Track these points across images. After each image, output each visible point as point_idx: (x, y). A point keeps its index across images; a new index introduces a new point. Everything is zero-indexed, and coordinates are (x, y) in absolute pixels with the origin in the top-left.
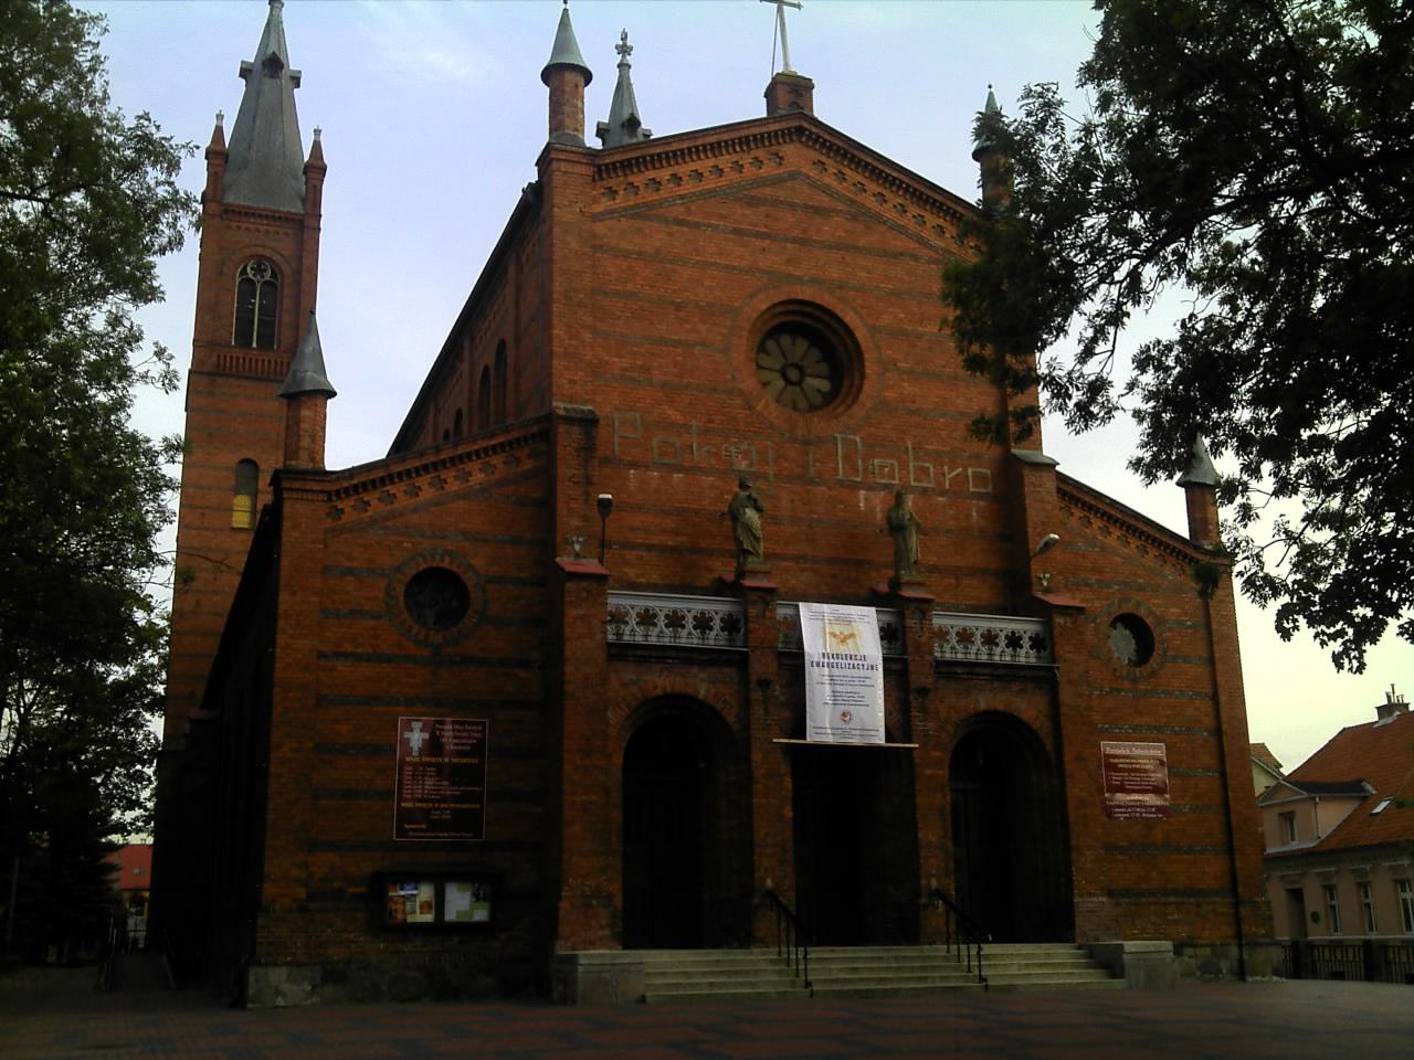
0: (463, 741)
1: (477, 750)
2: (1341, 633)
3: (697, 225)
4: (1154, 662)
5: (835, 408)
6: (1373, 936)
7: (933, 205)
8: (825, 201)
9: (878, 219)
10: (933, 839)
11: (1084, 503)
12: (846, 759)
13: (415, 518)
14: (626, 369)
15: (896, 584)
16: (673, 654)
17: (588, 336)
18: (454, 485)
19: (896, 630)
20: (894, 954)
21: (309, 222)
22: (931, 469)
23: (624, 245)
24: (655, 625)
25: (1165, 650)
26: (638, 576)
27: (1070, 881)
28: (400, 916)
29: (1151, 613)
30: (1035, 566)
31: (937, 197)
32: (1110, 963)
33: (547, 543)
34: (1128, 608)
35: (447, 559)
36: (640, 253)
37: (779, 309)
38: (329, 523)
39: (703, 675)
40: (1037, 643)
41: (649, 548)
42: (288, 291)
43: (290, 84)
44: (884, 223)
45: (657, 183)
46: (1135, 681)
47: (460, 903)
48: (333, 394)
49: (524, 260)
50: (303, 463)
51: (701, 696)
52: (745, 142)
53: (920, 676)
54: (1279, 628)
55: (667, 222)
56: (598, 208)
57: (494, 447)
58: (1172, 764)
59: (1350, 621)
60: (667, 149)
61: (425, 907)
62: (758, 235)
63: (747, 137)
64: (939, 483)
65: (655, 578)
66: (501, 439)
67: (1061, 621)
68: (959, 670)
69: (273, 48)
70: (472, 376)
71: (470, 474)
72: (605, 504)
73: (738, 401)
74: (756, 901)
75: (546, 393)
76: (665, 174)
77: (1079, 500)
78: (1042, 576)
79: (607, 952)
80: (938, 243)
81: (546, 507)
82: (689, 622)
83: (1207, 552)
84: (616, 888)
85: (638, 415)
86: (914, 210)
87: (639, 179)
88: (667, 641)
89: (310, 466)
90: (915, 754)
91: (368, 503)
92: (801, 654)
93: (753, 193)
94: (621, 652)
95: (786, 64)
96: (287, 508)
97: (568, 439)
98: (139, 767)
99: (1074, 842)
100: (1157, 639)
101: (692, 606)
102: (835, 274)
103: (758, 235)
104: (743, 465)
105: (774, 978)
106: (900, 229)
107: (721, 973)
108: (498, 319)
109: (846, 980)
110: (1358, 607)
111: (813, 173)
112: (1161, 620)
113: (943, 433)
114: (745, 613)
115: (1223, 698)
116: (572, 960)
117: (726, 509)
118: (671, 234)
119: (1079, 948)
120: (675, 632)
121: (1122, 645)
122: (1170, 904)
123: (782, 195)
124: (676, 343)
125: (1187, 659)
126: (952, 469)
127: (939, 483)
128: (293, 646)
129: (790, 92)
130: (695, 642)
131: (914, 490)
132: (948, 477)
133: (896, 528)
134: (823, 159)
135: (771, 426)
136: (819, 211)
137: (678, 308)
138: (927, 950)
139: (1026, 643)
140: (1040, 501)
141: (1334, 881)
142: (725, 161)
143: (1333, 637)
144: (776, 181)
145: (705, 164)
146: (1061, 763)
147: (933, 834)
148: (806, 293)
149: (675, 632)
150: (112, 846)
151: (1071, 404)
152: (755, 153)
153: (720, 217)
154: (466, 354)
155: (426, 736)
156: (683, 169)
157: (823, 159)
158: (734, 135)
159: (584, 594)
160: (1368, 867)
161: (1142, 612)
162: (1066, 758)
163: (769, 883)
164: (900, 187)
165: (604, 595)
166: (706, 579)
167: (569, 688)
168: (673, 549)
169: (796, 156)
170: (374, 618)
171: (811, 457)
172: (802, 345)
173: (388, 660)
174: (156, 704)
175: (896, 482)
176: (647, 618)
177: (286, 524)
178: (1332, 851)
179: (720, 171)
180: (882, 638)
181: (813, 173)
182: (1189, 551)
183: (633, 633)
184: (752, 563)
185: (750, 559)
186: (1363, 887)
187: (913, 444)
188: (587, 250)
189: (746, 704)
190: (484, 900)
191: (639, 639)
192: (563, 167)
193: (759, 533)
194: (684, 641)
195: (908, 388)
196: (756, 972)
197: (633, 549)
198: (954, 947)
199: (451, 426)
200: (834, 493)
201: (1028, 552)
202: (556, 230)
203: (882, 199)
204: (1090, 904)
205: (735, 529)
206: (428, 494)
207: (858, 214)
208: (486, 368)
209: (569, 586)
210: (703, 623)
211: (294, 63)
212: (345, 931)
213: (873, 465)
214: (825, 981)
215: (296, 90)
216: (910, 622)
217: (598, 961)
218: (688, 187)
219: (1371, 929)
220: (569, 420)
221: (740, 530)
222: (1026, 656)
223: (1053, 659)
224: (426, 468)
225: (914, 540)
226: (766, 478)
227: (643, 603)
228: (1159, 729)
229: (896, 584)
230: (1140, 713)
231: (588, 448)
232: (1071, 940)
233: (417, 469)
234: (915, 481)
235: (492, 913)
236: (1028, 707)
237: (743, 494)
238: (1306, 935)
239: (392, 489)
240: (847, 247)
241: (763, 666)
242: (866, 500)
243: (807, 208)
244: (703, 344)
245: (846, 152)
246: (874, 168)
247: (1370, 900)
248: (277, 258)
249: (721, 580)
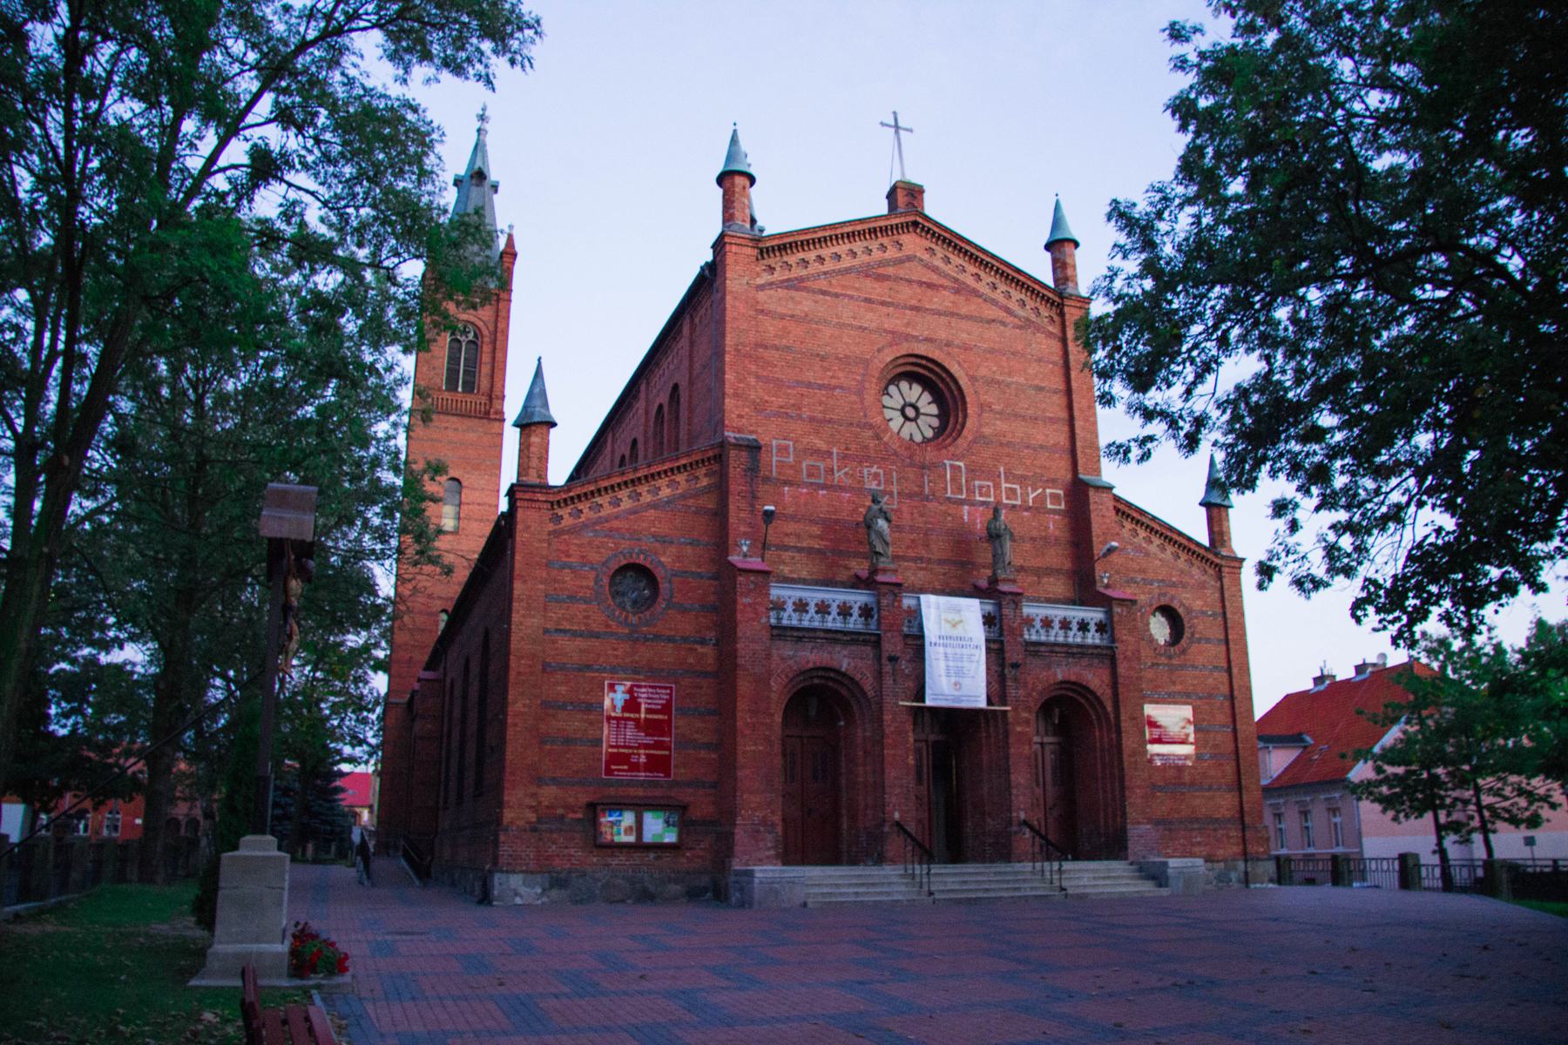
1: (666, 708)
2: (1398, 619)
3: (837, 295)
4: (1184, 642)
5: (944, 440)
6: (1340, 850)
7: (1017, 284)
8: (934, 278)
9: (975, 293)
10: (1022, 781)
11: (1133, 519)
12: (955, 721)
13: (616, 524)
14: (782, 407)
15: (994, 581)
16: (822, 635)
17: (752, 380)
19: (994, 618)
20: (993, 870)
21: (504, 296)
23: (780, 310)
24: (807, 612)
25: (1193, 634)
26: (791, 572)
27: (1124, 814)
28: (609, 837)
29: (1182, 604)
30: (1098, 567)
31: (1021, 278)
32: (1157, 876)
33: (722, 544)
34: (1164, 601)
35: (642, 556)
36: (792, 316)
37: (901, 361)
38: (551, 527)
39: (846, 652)
40: (1101, 628)
41: (800, 550)
42: (486, 349)
43: (491, 191)
44: (980, 296)
45: (805, 263)
46: (1170, 658)
47: (657, 828)
48: (554, 425)
49: (697, 320)
50: (532, 479)
51: (843, 669)
52: (873, 232)
53: (1013, 655)
54: (1353, 615)
55: (814, 292)
56: (760, 281)
57: (678, 468)
58: (1197, 722)
59: (1404, 610)
60: (814, 236)
61: (628, 830)
62: (883, 303)
63: (875, 229)
64: (1025, 501)
65: (804, 574)
66: (683, 462)
67: (1119, 610)
68: (1042, 649)
69: (479, 164)
70: (647, 412)
71: (659, 489)
72: (769, 516)
73: (870, 433)
74: (886, 829)
75: (721, 424)
76: (811, 255)
77: (1128, 516)
78: (1103, 577)
79: (771, 868)
80: (1021, 313)
81: (720, 515)
82: (834, 610)
83: (1223, 557)
84: (777, 818)
85: (791, 443)
86: (1002, 287)
87: (791, 259)
88: (816, 624)
89: (537, 481)
90: (1009, 715)
91: (581, 511)
92: (921, 637)
93: (881, 271)
95: (903, 174)
96: (520, 514)
97: (737, 462)
98: (365, 713)
99: (1127, 784)
100: (1187, 625)
101: (835, 597)
102: (942, 335)
103: (883, 303)
104: (873, 486)
105: (903, 888)
106: (994, 302)
107: (863, 885)
108: (671, 367)
109: (958, 891)
111: (926, 257)
112: (1189, 610)
113: (1028, 462)
114: (879, 603)
115: (1235, 671)
116: (750, 874)
117: (861, 519)
118: (816, 302)
119: (1131, 864)
120: (823, 617)
121: (1159, 629)
122: (1194, 829)
123: (902, 273)
124: (821, 387)
125: (1208, 640)
126: (1034, 490)
127: (1025, 501)
128: (526, 624)
129: (905, 196)
130: (839, 625)
131: (1006, 506)
132: (1031, 496)
133: (994, 536)
134: (933, 246)
135: (895, 454)
136: (930, 286)
137: (823, 359)
138: (1018, 866)
139: (1092, 628)
140: (1101, 516)
141: (1283, 810)
142: (858, 246)
143: (1392, 622)
144: (898, 262)
145: (842, 248)
146: (1117, 717)
147: (1020, 777)
148: (921, 349)
149: (823, 617)
150: (341, 774)
151: (1182, 433)
152: (881, 240)
153: (857, 289)
154: (642, 395)
155: (627, 696)
156: (826, 252)
157: (933, 246)
158: (866, 226)
159: (752, 586)
160: (1308, 799)
161: (1175, 604)
162: (1123, 718)
163: (897, 815)
164: (992, 268)
165: (766, 587)
166: (843, 575)
167: (741, 661)
168: (819, 551)
169: (913, 243)
170: (585, 602)
172: (917, 389)
173: (597, 636)
174: (379, 666)
175: (992, 499)
176: (801, 607)
177: (519, 527)
178: (1281, 788)
179: (853, 254)
180: (984, 624)
181: (926, 257)
182: (1210, 556)
183: (790, 618)
184: (883, 562)
185: (882, 559)
186: (1305, 814)
188: (752, 313)
189: (879, 675)
190: (674, 825)
191: (795, 623)
192: (734, 248)
193: (888, 539)
194: (830, 625)
195: (1001, 425)
196: (890, 884)
197: (786, 550)
198: (1038, 865)
199: (627, 454)
200: (943, 508)
201: (1093, 555)
202: (728, 298)
203: (978, 277)
204: (1140, 833)
205: (869, 535)
207: (959, 289)
208: (661, 406)
209: (740, 579)
210: (845, 611)
211: (494, 175)
212: (567, 847)
214: (943, 891)
215: (495, 196)
216: (1006, 611)
217: (771, 875)
218: (829, 265)
219: (1338, 845)
220: (738, 446)
221: (873, 536)
222: (1093, 638)
223: (1113, 640)
225: (1008, 545)
226: (891, 494)
228: (1188, 695)
229: (994, 581)
230: (1174, 683)
231: (753, 470)
232: (1126, 858)
233: (619, 485)
234: (1007, 498)
235: (680, 836)
236: (1096, 679)
237: (875, 507)
239: (598, 500)
240: (953, 314)
241: (891, 646)
243: (921, 283)
244: (841, 388)
245: (951, 242)
246: (972, 254)
247: (1309, 824)
248: (480, 324)
249: (857, 576)
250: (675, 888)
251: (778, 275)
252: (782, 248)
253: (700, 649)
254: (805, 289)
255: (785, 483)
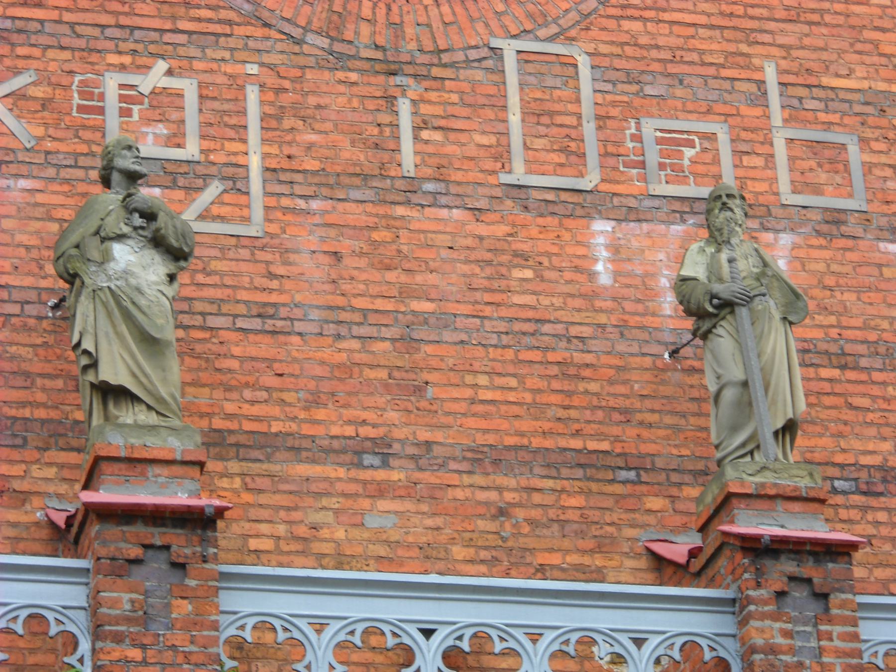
0: (735, 22)
22: (853, 150)
171: (404, 107)
187: (781, 72)
213: (637, 138)
242: (615, 248)
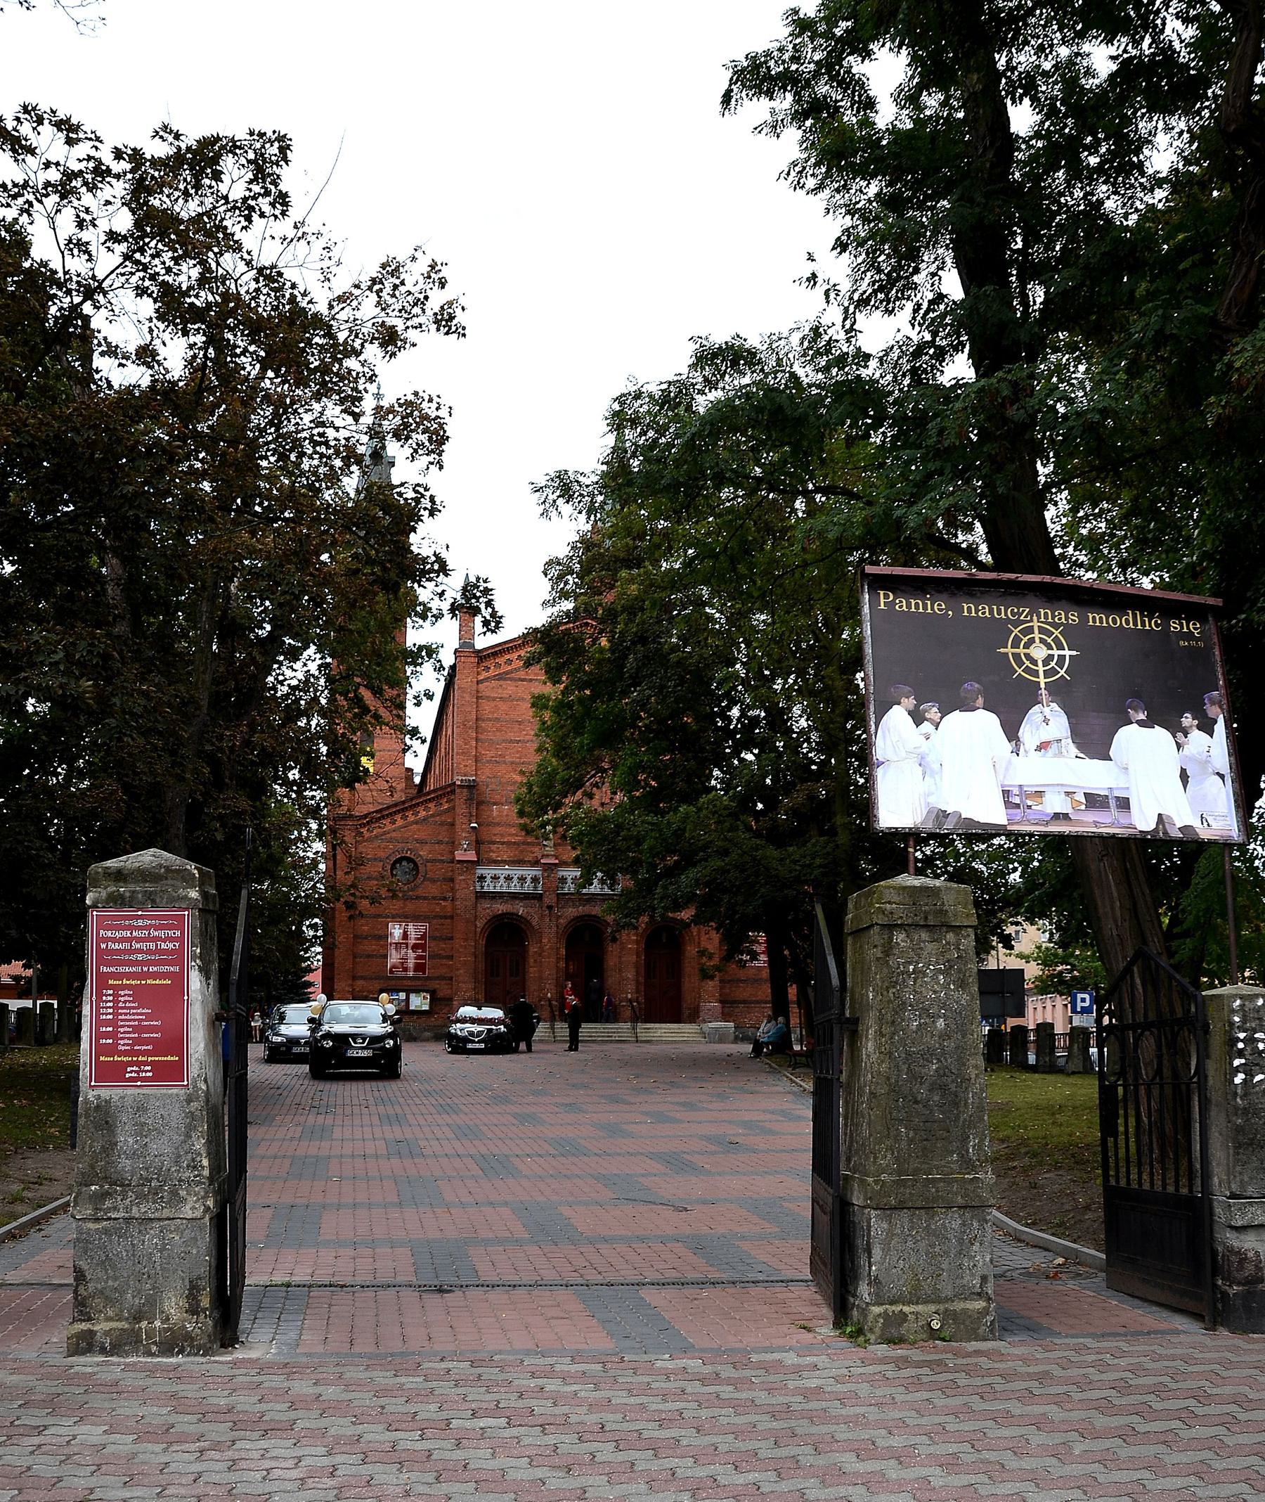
3: (531, 680)
13: (394, 835)
18: (411, 818)
41: (503, 843)
55: (516, 680)
56: (481, 678)
65: (505, 857)
87: (501, 660)
94: (482, 895)
101: (516, 872)
110: (917, 335)
137: (520, 723)
138: (621, 1025)
166: (529, 858)
183: (489, 887)
206: (400, 822)
210: (522, 879)
224: (399, 811)
227: (508, 872)
238: (888, 1210)
250: (427, 1034)
251: (492, 672)
252: (495, 654)
253: (443, 904)
254: (510, 679)
255: (495, 804)
